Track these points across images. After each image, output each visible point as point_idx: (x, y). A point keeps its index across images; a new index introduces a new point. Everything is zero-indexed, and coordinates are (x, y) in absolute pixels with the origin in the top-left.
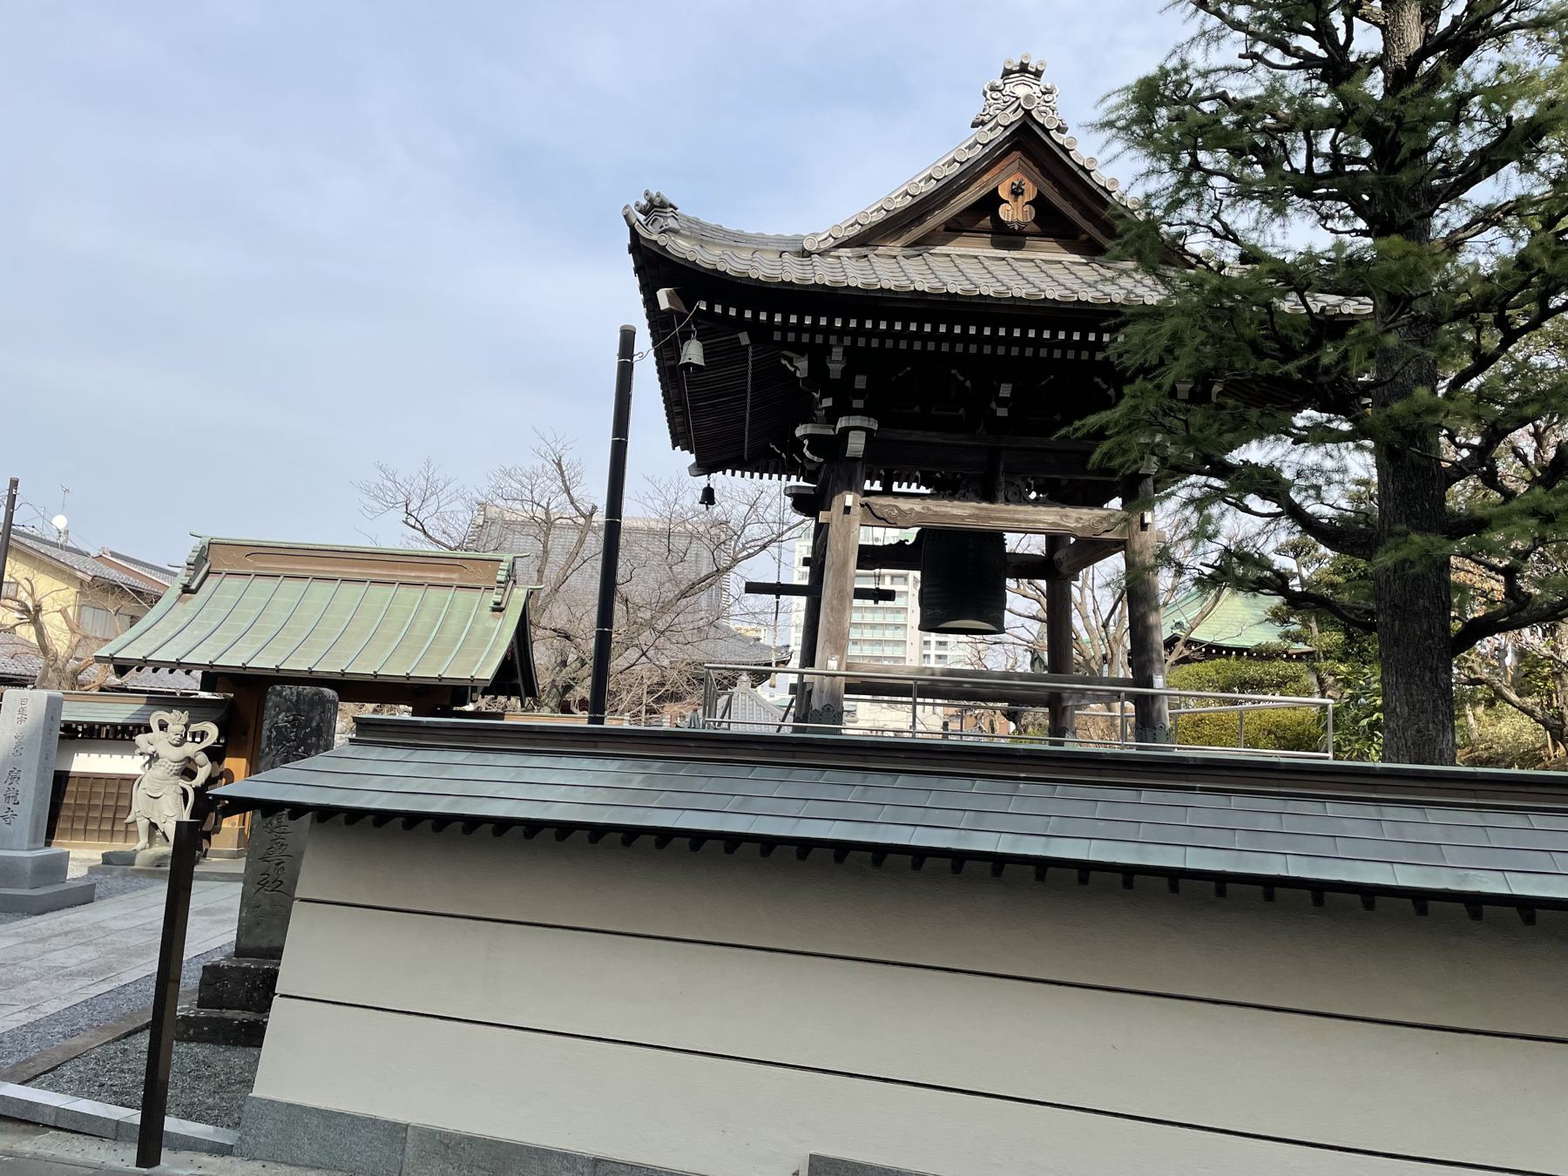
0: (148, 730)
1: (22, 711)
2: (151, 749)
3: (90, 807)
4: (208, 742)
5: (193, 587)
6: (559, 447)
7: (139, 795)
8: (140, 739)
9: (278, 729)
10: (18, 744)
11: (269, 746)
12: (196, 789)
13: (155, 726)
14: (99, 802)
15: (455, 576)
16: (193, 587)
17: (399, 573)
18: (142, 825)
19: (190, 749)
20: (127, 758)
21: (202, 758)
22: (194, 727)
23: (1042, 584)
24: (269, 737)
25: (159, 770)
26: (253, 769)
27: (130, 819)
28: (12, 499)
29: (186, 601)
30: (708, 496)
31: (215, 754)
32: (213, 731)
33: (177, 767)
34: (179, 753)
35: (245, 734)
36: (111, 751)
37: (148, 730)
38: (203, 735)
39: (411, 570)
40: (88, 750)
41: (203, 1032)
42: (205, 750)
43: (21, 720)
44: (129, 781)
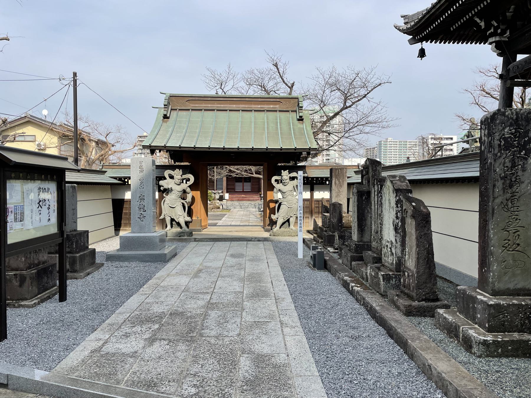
0: (165, 179)
1: (141, 167)
4: (189, 183)
6: (275, 58)
9: (505, 139)
10: (142, 183)
11: (500, 151)
15: (277, 106)
16: (168, 115)
17: (253, 106)
19: (184, 186)
21: (188, 190)
22: (184, 177)
24: (500, 145)
28: (75, 81)
29: (166, 122)
30: (422, 53)
31: (193, 187)
37: (165, 179)
38: (188, 180)
39: (258, 104)
41: (508, 351)
43: (141, 171)
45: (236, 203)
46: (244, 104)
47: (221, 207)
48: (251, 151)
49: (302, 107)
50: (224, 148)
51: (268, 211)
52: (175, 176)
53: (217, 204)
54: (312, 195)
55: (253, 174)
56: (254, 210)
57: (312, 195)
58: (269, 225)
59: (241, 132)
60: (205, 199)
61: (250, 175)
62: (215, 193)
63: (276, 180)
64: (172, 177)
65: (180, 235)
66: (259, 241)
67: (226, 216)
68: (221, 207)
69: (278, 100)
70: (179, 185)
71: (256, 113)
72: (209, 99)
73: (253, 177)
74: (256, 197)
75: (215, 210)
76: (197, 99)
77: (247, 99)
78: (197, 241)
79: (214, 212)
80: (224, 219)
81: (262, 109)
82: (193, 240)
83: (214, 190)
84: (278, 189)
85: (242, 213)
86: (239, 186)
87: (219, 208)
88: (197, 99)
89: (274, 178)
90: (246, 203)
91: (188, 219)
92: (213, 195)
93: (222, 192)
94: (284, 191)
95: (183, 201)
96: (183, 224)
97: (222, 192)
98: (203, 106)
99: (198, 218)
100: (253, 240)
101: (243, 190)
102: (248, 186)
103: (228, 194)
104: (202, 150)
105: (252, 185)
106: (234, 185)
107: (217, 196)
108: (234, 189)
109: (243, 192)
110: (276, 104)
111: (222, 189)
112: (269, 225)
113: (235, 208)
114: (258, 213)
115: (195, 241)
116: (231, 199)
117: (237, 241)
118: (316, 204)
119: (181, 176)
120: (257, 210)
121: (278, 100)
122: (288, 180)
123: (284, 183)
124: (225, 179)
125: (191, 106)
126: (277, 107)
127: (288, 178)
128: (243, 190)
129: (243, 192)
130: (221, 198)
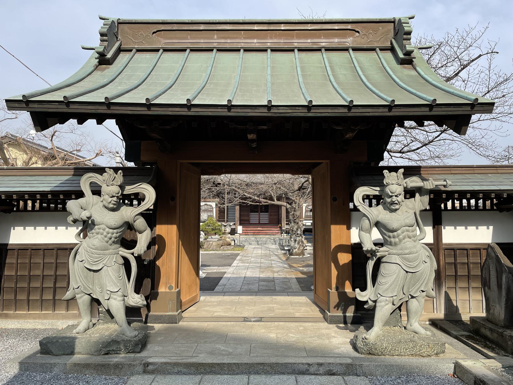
2: (84, 215)
3: (30, 278)
5: (109, 56)
7: (76, 268)
8: (72, 205)
12: (138, 258)
13: (86, 189)
14: (38, 272)
16: (109, 56)
18: (83, 300)
19: (128, 213)
20: (61, 229)
21: (141, 223)
22: (129, 190)
23: (152, 208)
25: (96, 239)
26: (245, 233)
27: (68, 295)
31: (151, 218)
32: (150, 194)
33: (116, 234)
34: (115, 219)
35: (173, 199)
36: (46, 224)
37: (80, 195)
39: (306, 37)
40: (24, 223)
42: (142, 214)
44: (66, 250)
45: (252, 238)
46: (276, 37)
47: (233, 244)
48: (302, 113)
49: (409, 33)
50: (229, 107)
51: (334, 273)
52: (105, 189)
53: (228, 240)
54: (438, 236)
55: (274, 201)
56: (274, 247)
57: (438, 236)
58: (337, 306)
59: (272, 84)
60: (191, 244)
61: (270, 202)
62: (225, 226)
63: (367, 197)
64: (97, 192)
65: (109, 347)
66: (331, 373)
67: (239, 258)
68: (233, 244)
69: (349, 27)
70: (113, 210)
71: (304, 55)
72: (202, 27)
73: (273, 205)
74: (276, 230)
75: (225, 247)
76: (175, 27)
77: (283, 27)
78: (152, 372)
79: (224, 250)
80: (235, 263)
81: (315, 46)
82: (140, 369)
83: (224, 221)
84: (373, 222)
85: (259, 252)
86: (254, 217)
87: (230, 245)
88: (175, 27)
89: (360, 192)
90: (264, 238)
91: (137, 300)
92: (223, 228)
93: (235, 224)
94: (394, 225)
95: (126, 253)
96: (120, 314)
97: (235, 224)
98: (189, 41)
99: (170, 288)
100: (312, 370)
101: (259, 221)
102: (265, 217)
103: (241, 227)
104: (169, 112)
105: (270, 215)
106: (248, 216)
107: (228, 230)
108: (249, 220)
109: (259, 224)
110: (345, 37)
111: (234, 220)
112: (337, 306)
113: (250, 244)
114: (279, 251)
115: (145, 372)
116: (245, 233)
117: (267, 373)
118: (449, 256)
119: (122, 187)
120: (278, 246)
121: (349, 27)
122: (401, 198)
123: (393, 203)
124: (238, 208)
125: (161, 42)
126: (349, 41)
127: (400, 190)
128: (259, 221)
129: (259, 223)
130: (233, 232)
